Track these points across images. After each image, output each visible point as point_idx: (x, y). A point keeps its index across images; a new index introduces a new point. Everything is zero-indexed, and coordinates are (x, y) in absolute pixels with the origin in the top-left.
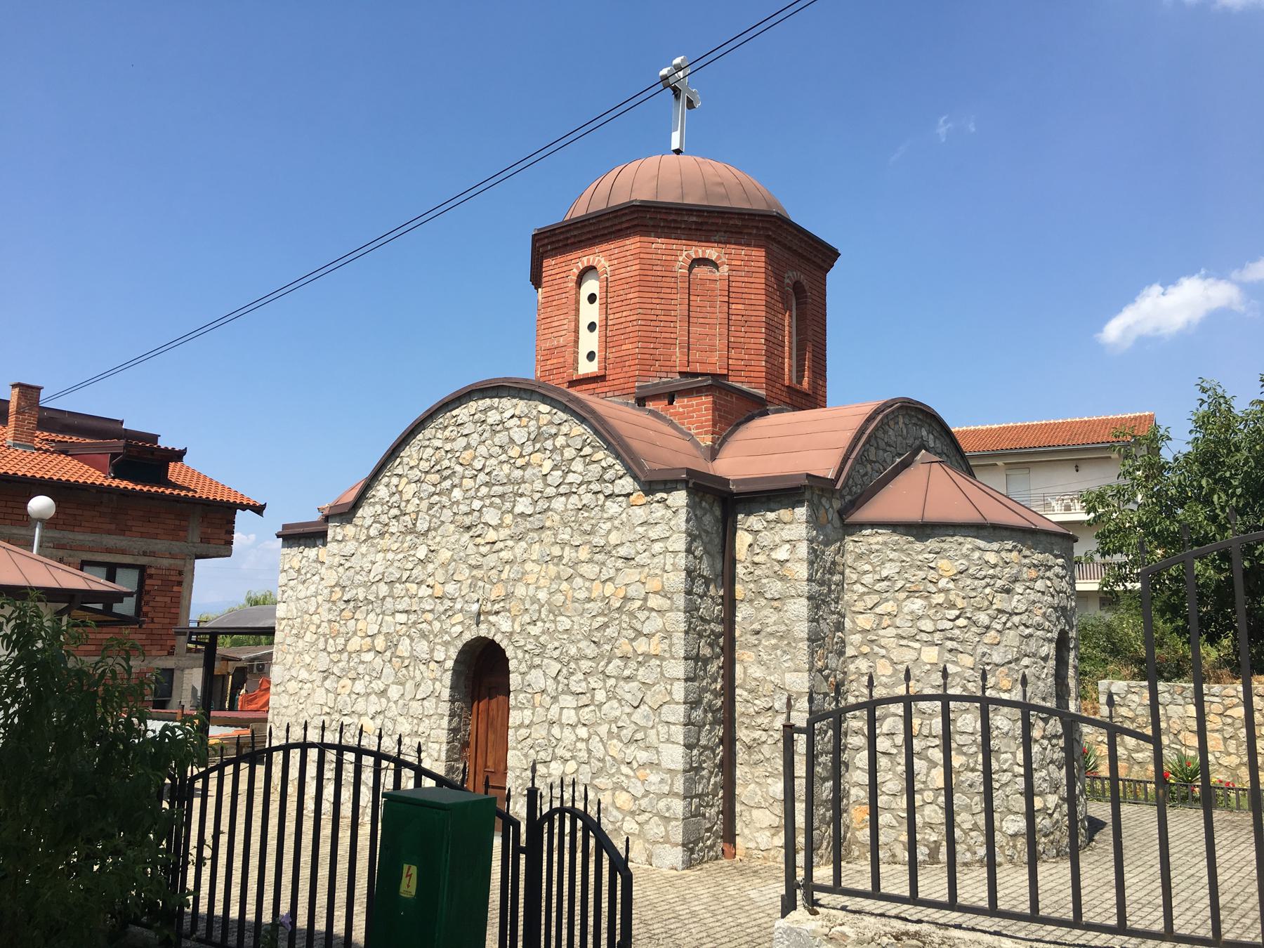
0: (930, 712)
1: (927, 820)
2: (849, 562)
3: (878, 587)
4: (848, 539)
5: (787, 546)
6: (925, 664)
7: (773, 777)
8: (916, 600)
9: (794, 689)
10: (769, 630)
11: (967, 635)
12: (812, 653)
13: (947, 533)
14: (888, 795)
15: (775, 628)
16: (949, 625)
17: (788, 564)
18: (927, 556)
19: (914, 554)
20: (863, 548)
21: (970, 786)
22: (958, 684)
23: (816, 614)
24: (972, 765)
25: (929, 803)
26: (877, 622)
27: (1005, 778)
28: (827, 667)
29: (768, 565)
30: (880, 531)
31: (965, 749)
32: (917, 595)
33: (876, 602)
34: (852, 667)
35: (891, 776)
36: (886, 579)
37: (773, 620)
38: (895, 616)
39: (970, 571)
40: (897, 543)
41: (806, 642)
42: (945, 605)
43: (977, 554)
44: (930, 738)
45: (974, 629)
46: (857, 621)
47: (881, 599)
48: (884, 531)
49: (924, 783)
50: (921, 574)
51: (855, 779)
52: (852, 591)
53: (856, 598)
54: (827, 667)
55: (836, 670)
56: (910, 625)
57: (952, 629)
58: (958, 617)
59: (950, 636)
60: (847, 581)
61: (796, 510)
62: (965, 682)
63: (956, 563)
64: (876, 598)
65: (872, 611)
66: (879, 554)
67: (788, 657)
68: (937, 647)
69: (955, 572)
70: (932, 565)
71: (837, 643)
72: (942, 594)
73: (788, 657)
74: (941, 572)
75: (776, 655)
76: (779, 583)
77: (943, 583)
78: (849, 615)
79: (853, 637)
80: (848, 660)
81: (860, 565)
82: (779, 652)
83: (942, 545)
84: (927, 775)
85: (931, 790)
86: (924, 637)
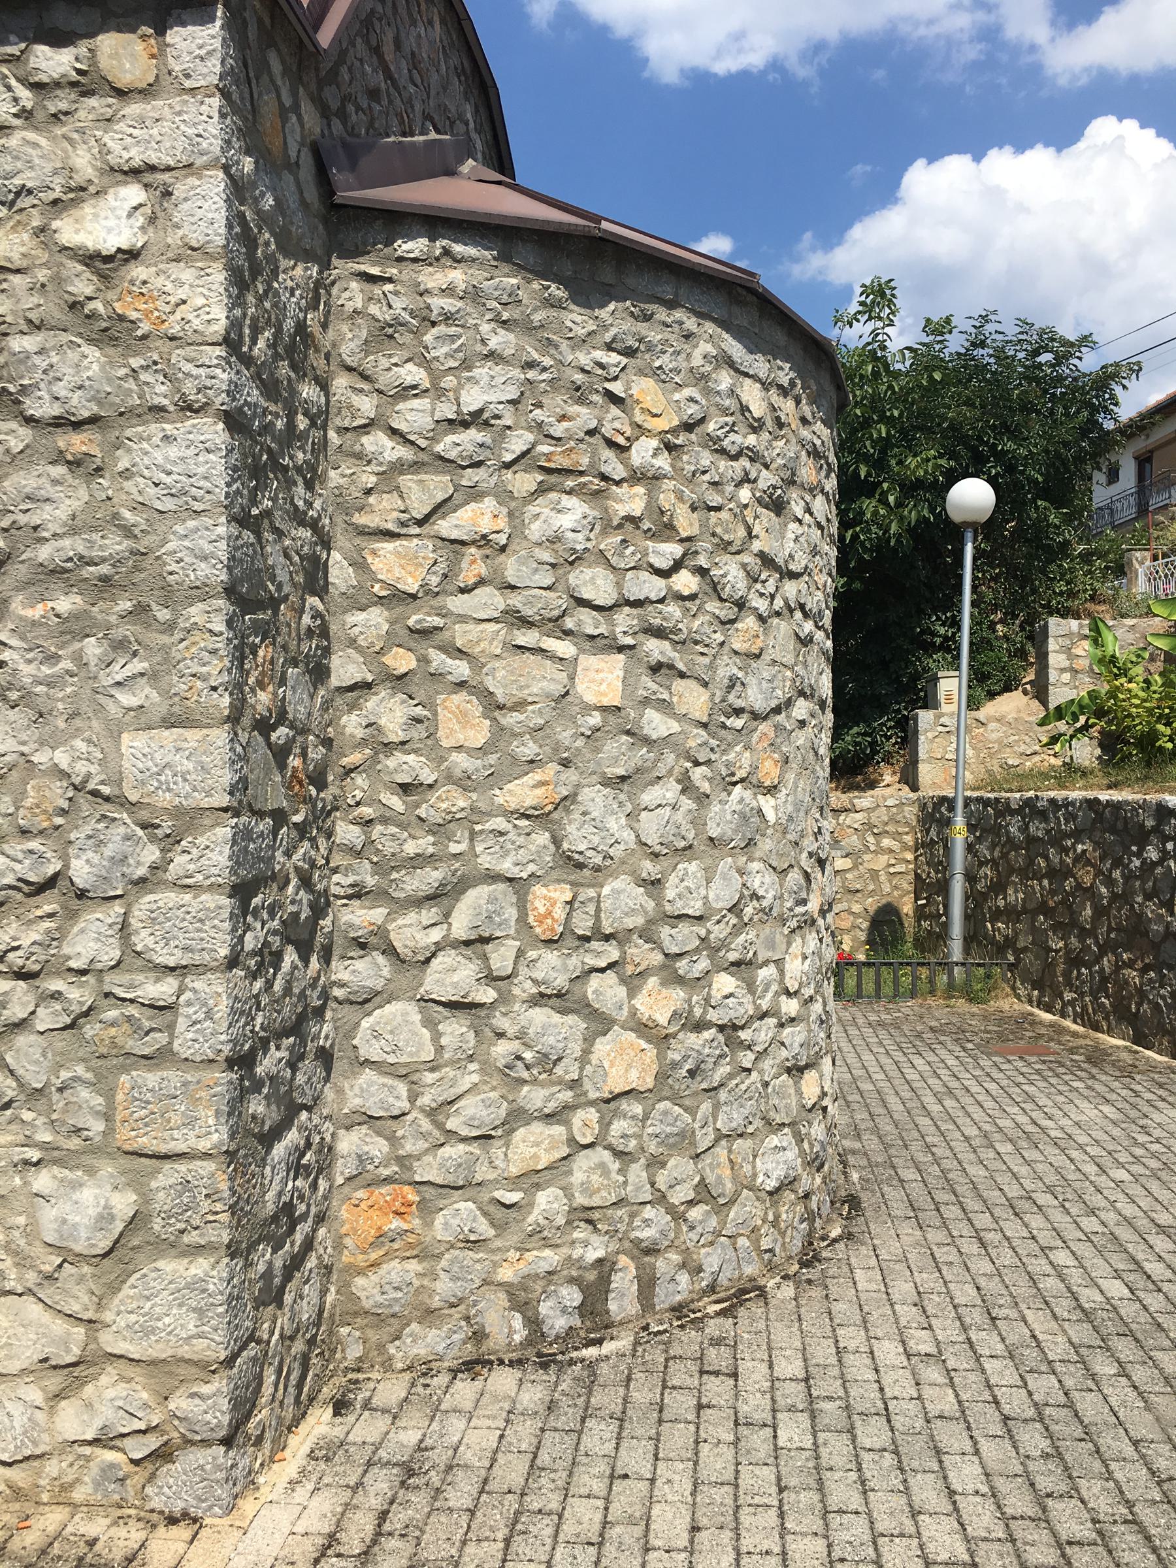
0: (598, 860)
1: (580, 1200)
2: (349, 350)
3: (447, 445)
4: (341, 267)
5: (133, 193)
6: (588, 709)
7: (57, 1162)
8: (568, 501)
9: (165, 799)
10: (44, 553)
11: (697, 623)
12: (241, 653)
13: (658, 290)
14: (465, 1140)
15: (72, 546)
16: (654, 587)
17: (139, 271)
18: (600, 355)
19: (564, 346)
20: (398, 303)
21: (692, 1073)
22: (670, 772)
23: (254, 502)
24: (698, 1012)
25: (586, 1147)
26: (442, 567)
27: (763, 1034)
28: (282, 718)
29: (42, 275)
30: (458, 248)
31: (682, 965)
32: (570, 483)
33: (440, 496)
34: (352, 724)
35: (475, 1078)
36: (476, 419)
37: (63, 513)
38: (503, 549)
39: (711, 427)
40: (513, 301)
41: (221, 603)
42: (646, 525)
43: (724, 380)
44: (595, 945)
45: (712, 606)
46: (375, 564)
47: (457, 488)
48: (471, 251)
49: (575, 1084)
50: (585, 417)
51: (354, 1102)
52: (359, 456)
53: (372, 480)
54: (282, 718)
55: (304, 731)
56: (547, 582)
57: (661, 601)
58: (677, 566)
59: (657, 622)
60: (338, 421)
61: (176, 36)
62: (688, 765)
63: (677, 396)
64: (438, 485)
65: (426, 529)
66: (453, 330)
67: (137, 666)
68: (621, 657)
69: (676, 422)
70: (617, 388)
71: (310, 632)
72: (640, 490)
73: (137, 666)
74: (639, 418)
75: (79, 659)
76: (92, 352)
77: (644, 452)
78: (341, 540)
79: (359, 617)
80: (339, 701)
81: (384, 363)
82: (92, 648)
83: (642, 328)
84: (584, 1059)
85: (592, 1103)
86: (588, 622)
